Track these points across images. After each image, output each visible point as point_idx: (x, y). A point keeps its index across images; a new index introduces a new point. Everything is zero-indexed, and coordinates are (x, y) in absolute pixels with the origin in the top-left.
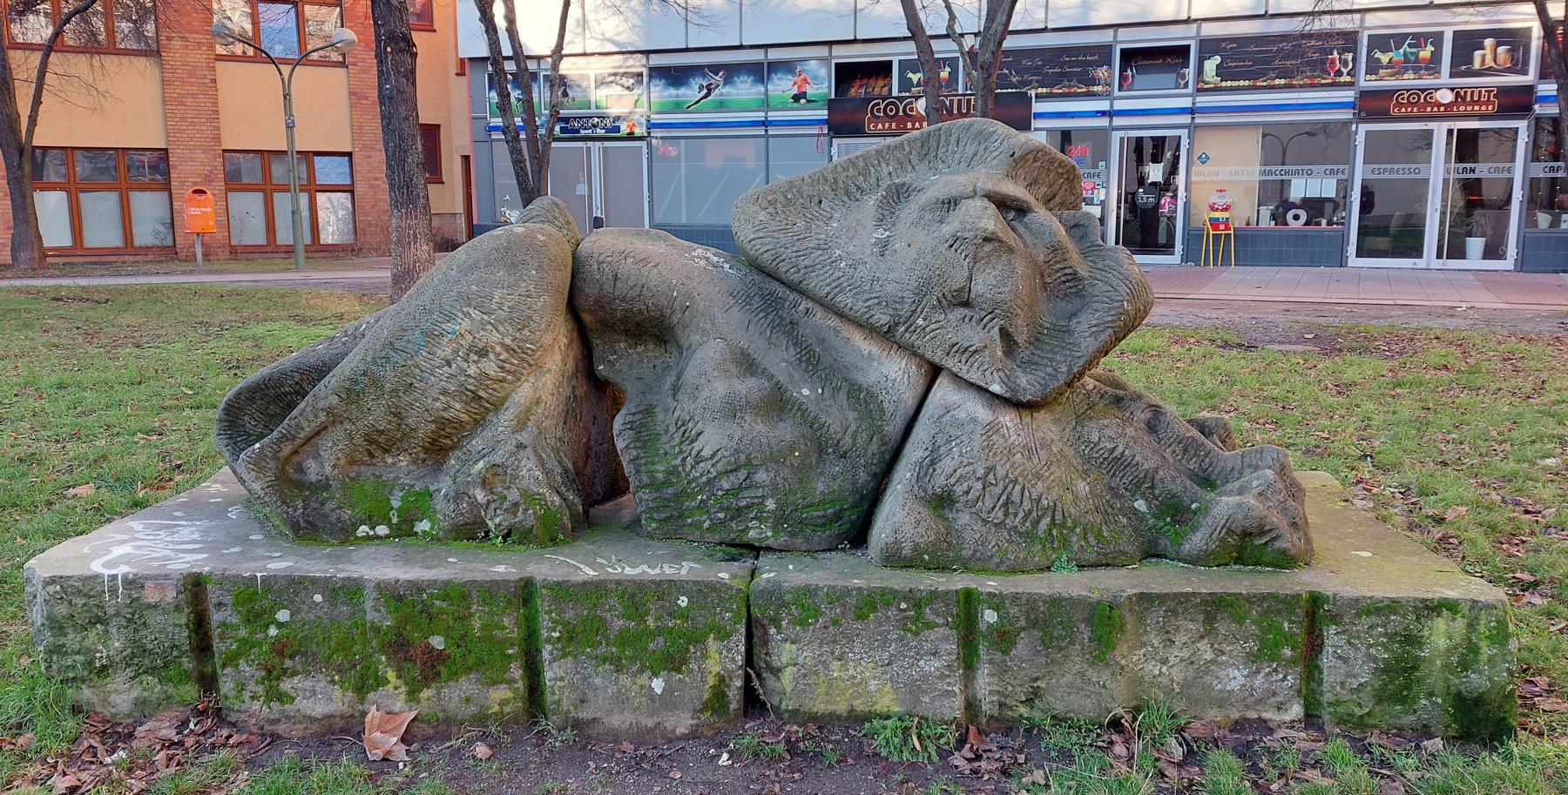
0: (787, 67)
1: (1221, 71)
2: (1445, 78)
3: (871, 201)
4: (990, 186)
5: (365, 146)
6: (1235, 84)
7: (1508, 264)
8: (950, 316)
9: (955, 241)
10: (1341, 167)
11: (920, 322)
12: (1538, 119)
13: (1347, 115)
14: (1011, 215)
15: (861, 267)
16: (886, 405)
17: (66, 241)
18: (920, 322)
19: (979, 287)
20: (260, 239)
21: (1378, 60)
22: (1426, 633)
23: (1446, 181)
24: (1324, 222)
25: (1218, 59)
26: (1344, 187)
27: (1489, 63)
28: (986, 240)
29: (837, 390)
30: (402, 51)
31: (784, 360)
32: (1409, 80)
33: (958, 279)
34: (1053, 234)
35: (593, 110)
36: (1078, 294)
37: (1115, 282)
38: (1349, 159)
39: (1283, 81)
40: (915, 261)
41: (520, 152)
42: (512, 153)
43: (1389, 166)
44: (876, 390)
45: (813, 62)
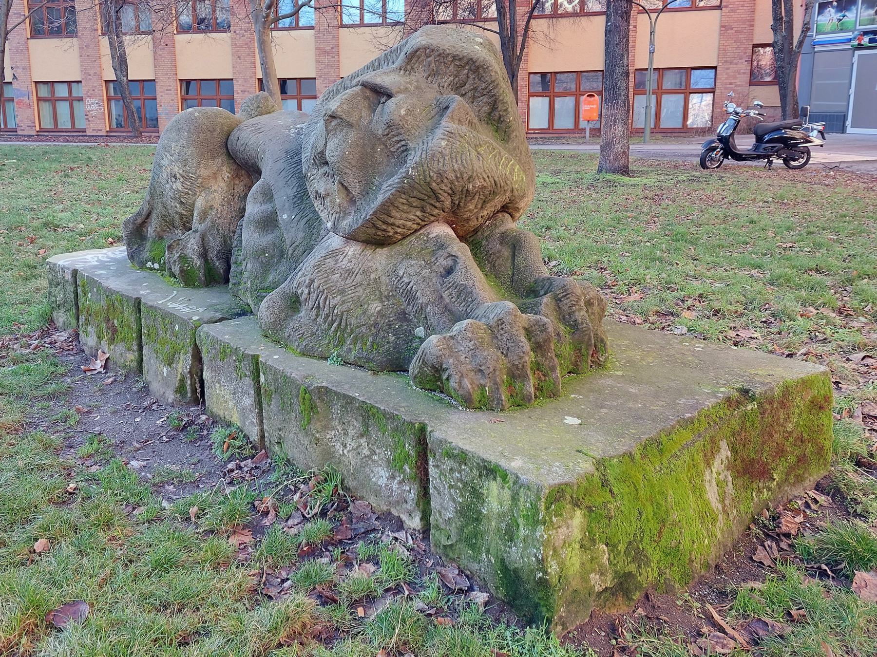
17: (69, 126)
20: (570, 125)
22: (485, 492)
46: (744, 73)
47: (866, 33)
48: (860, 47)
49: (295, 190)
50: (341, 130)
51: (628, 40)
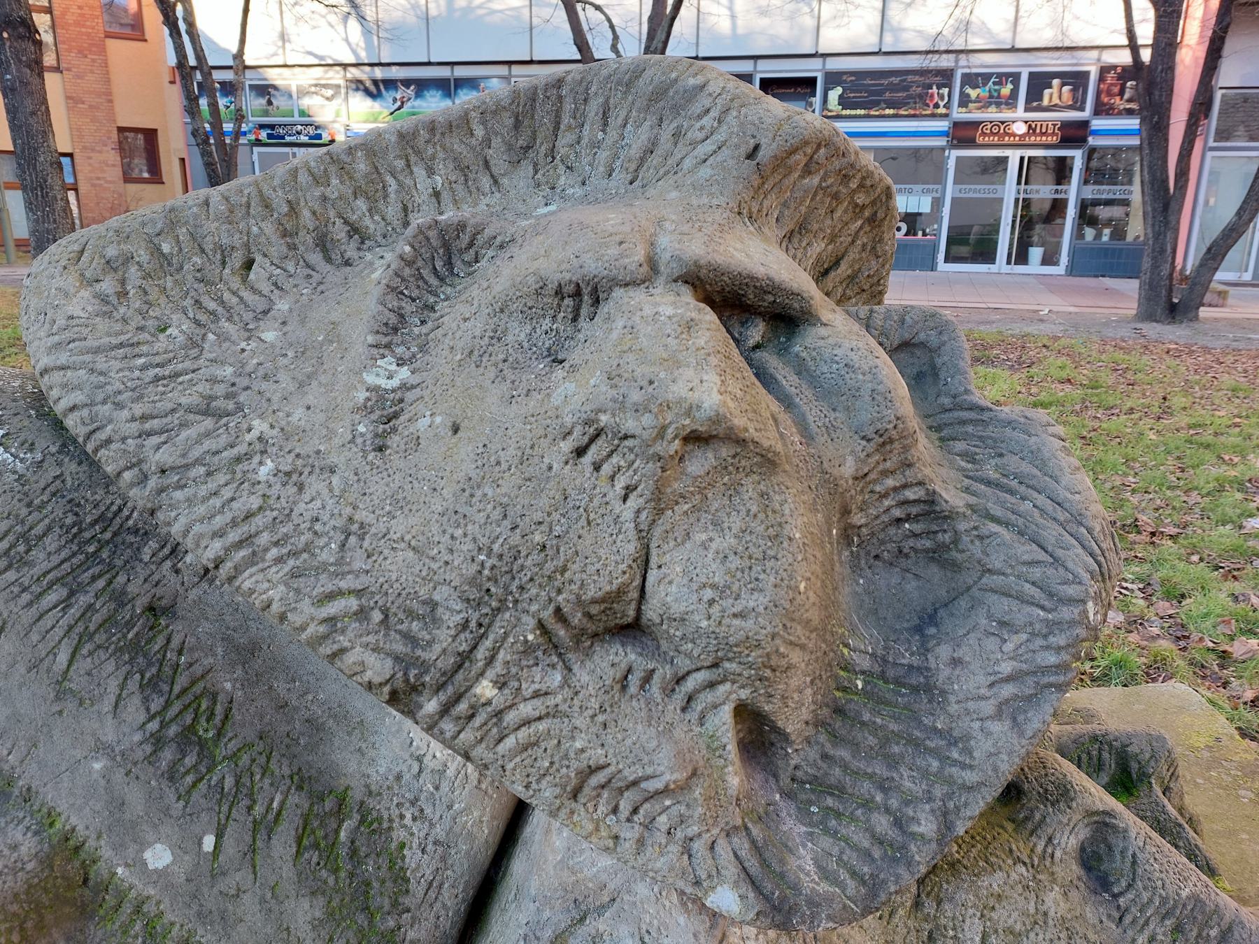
0: (472, 83)
1: (843, 102)
2: (1020, 112)
3: (379, 267)
4: (697, 249)
5: (85, 148)
6: (853, 112)
7: (1060, 269)
8: (582, 675)
9: (591, 439)
10: (936, 187)
11: (485, 689)
12: (1093, 150)
13: (941, 142)
14: (756, 332)
15: (315, 485)
16: (412, 857)
18: (485, 689)
19: (671, 593)
21: (968, 95)
23: (1017, 200)
24: (920, 233)
25: (839, 90)
26: (937, 203)
27: (1056, 100)
28: (695, 439)
29: (264, 827)
30: (21, 37)
31: (102, 748)
32: (992, 114)
33: (602, 564)
34: (881, 397)
35: (297, 118)
36: (938, 555)
37: (1051, 533)
38: (940, 179)
39: (891, 112)
40: (469, 488)
41: (211, 154)
42: (203, 155)
43: (972, 187)
44: (384, 807)
45: (495, 80)
46: (114, 166)
47: (262, 126)
48: (258, 143)
49: (134, 711)
50: (734, 489)
51: (47, 108)
